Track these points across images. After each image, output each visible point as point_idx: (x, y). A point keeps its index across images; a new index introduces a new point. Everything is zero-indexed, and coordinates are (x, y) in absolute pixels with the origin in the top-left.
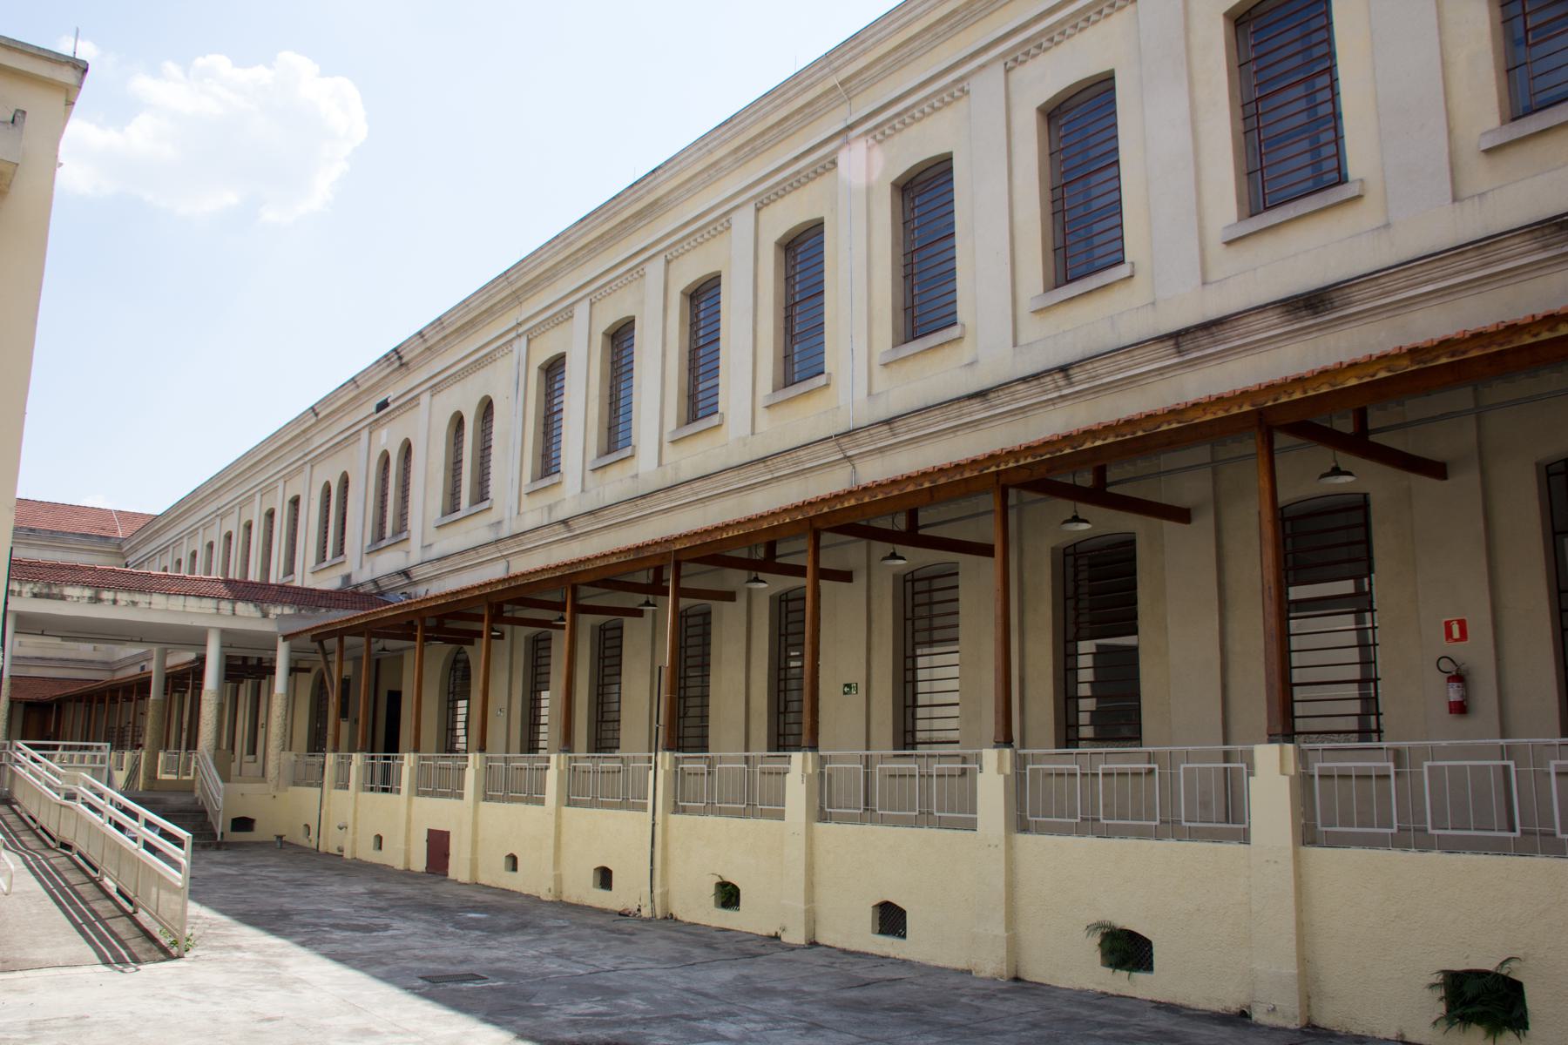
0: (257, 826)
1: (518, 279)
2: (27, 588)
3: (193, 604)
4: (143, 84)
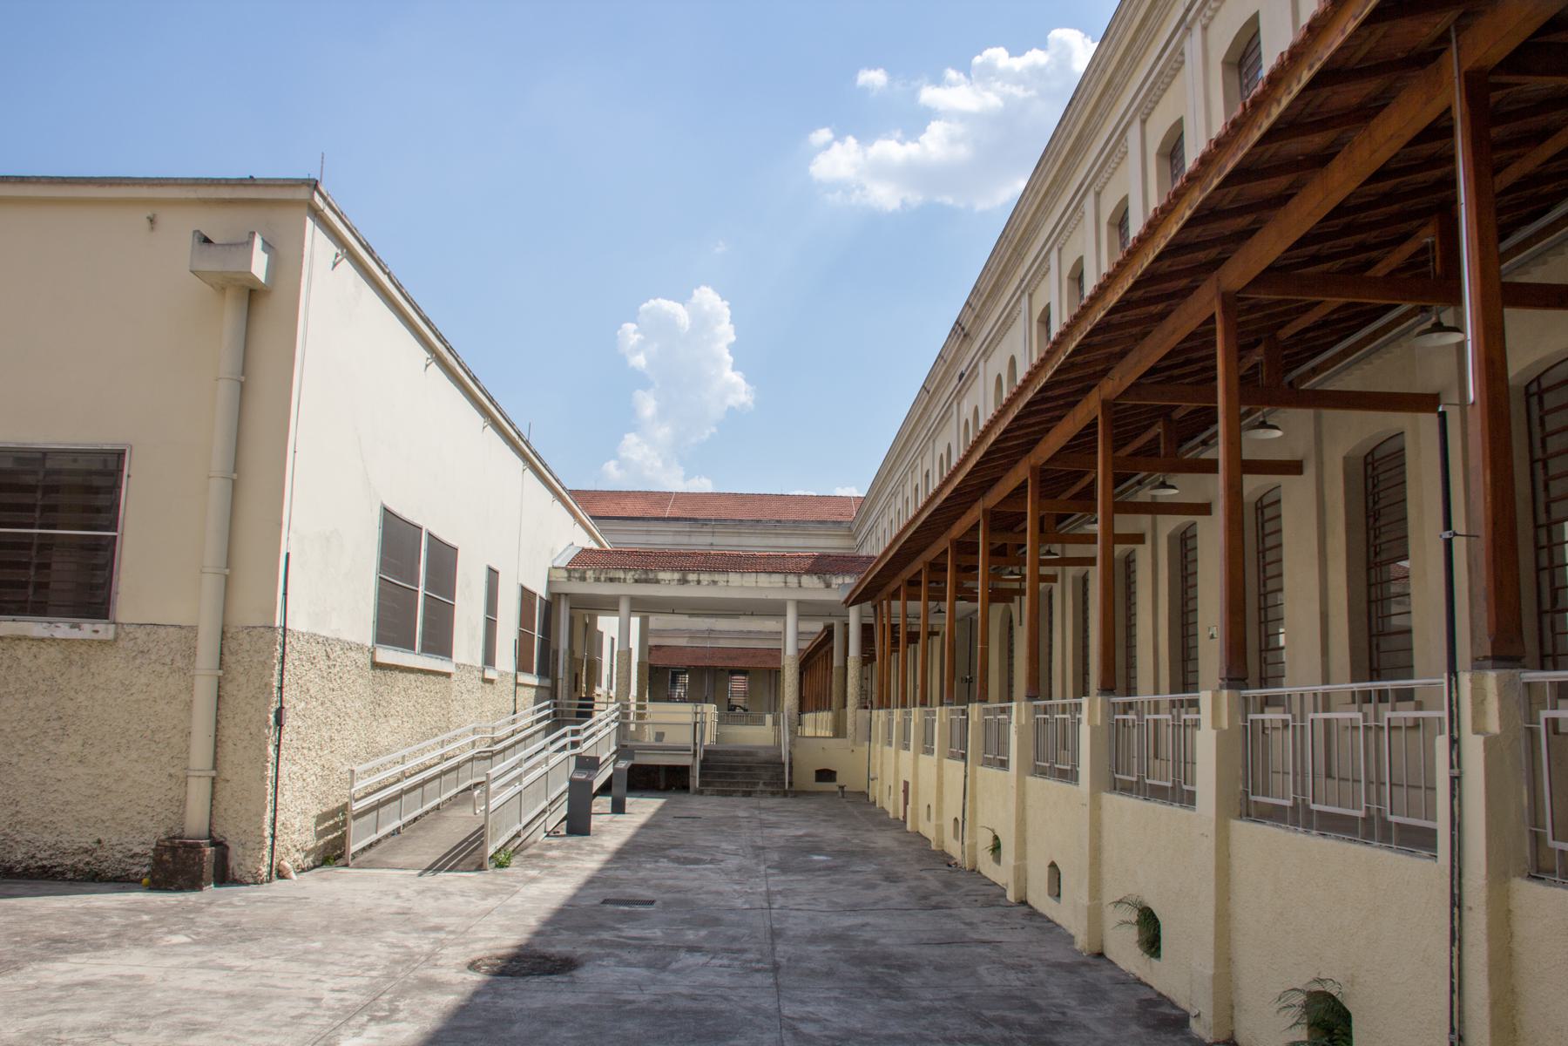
2: (630, 576)
3: (764, 580)
4: (930, 95)
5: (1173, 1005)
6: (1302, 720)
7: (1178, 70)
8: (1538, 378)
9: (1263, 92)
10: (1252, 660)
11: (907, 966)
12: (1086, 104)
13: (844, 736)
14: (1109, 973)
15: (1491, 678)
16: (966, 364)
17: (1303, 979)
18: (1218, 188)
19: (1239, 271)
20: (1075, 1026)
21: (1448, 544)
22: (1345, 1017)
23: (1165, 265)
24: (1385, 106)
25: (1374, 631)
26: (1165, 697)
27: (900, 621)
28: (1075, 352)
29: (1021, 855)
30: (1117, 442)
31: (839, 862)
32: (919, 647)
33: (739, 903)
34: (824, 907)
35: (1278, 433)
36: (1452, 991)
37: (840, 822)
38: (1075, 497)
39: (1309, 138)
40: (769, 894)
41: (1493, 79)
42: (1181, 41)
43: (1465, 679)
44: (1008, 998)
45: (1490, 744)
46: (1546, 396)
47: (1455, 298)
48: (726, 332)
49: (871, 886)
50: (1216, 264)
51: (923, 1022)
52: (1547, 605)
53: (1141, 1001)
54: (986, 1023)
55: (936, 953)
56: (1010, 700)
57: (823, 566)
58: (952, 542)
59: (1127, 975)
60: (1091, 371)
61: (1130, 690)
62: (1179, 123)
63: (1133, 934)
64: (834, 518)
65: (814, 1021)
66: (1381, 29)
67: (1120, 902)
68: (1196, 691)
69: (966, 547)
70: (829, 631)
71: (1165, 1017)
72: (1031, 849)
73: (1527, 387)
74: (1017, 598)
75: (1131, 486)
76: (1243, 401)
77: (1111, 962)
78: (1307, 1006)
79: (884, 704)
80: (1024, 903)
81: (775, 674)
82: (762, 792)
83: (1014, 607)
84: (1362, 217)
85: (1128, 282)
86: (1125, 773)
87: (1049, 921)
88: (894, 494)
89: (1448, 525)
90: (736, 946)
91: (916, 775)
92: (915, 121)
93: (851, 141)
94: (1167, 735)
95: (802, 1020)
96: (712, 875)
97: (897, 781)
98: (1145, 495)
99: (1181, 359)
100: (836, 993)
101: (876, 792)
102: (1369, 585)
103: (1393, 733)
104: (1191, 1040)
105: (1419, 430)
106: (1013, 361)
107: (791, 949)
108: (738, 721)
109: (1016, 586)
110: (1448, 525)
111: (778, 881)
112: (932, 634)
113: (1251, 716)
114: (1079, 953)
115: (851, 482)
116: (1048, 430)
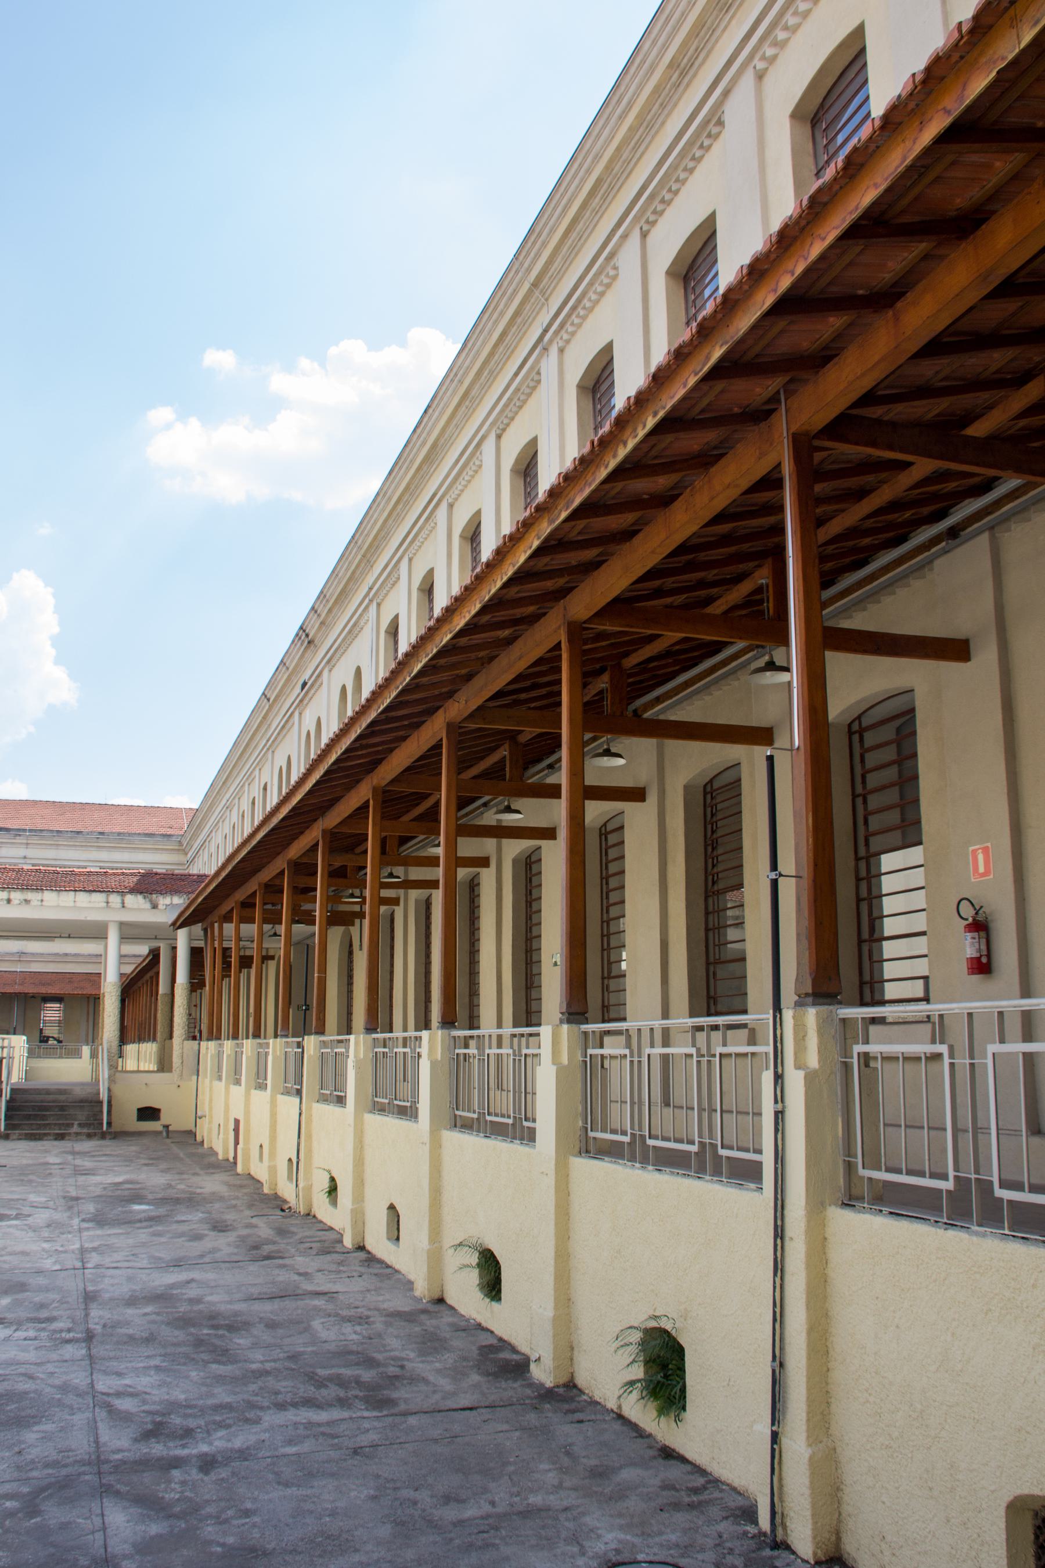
0: (162, 1115)
1: (364, 542)
3: (83, 898)
4: (280, 382)
5: (514, 1350)
6: (639, 1056)
7: (534, 388)
8: (859, 717)
9: (611, 432)
10: (593, 995)
11: (236, 1325)
12: (441, 413)
13: (170, 1070)
14: (450, 1319)
15: (811, 1014)
16: (309, 672)
17: (640, 1317)
18: (567, 520)
19: (588, 599)
20: (414, 1379)
21: (775, 884)
22: (678, 1351)
23: (513, 592)
24: (722, 455)
25: (712, 959)
26: (508, 1030)
27: (232, 945)
28: (421, 673)
29: (359, 1196)
30: (461, 765)
31: (162, 1211)
32: (253, 971)
33: (48, 1264)
34: (145, 1263)
35: (621, 762)
36: (775, 1320)
37: (163, 1165)
38: (419, 818)
39: (655, 478)
40: (83, 1251)
41: (816, 443)
42: (537, 361)
43: (788, 1015)
44: (344, 1354)
45: (811, 1079)
46: (866, 735)
47: (785, 642)
48: (49, 622)
49: (197, 1237)
50: (563, 593)
51: (253, 1387)
52: (865, 935)
53: (481, 1348)
54: (321, 1383)
55: (266, 1308)
56: (349, 1033)
57: (150, 884)
58: (289, 862)
59: (467, 1320)
60: (437, 692)
61: (473, 1022)
62: (533, 443)
63: (473, 1277)
64: (163, 831)
65: (132, 1395)
66: (720, 385)
67: (460, 1244)
68: (539, 1025)
69: (304, 868)
70: (155, 955)
71: (505, 1363)
72: (369, 1192)
73: (850, 725)
74: (357, 921)
75: (478, 808)
76: (586, 728)
77: (452, 1308)
78: (643, 1343)
79: (215, 1034)
80: (361, 1248)
81: (93, 1001)
82: (77, 1134)
83: (354, 931)
84: (703, 556)
85: (475, 607)
86: (463, 1114)
87: (388, 1267)
88: (229, 807)
89: (774, 866)
90: (44, 1314)
91: (247, 1113)
92: (265, 409)
93: (194, 423)
94: (509, 1066)
95: (119, 1394)
96: (18, 1233)
97: (227, 1120)
98: (490, 818)
99: (528, 683)
100: (157, 1361)
101: (203, 1131)
102: (707, 913)
103: (724, 1061)
104: (531, 1385)
105: (751, 759)
106: (358, 672)
107: (106, 1314)
108: (50, 1054)
109: (357, 908)
110: (774, 866)
111: (94, 1236)
112: (267, 958)
113: (590, 1051)
114: (419, 1300)
115: (186, 794)
116: (391, 750)
